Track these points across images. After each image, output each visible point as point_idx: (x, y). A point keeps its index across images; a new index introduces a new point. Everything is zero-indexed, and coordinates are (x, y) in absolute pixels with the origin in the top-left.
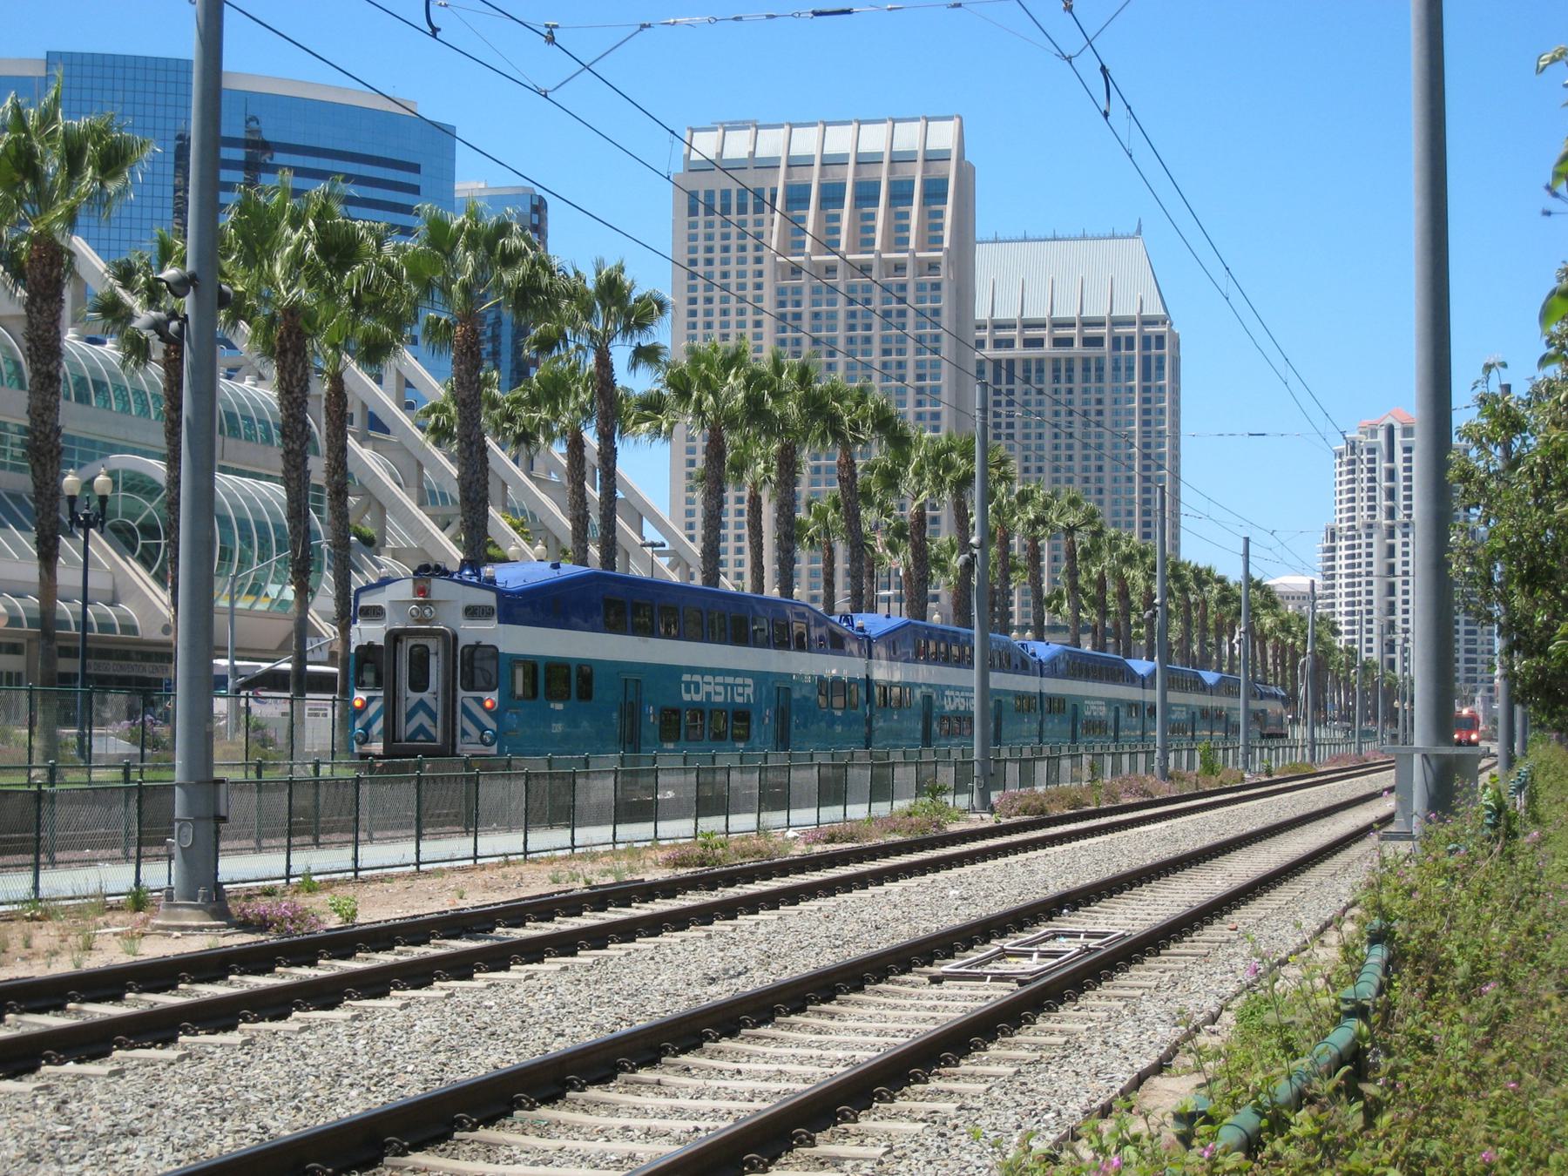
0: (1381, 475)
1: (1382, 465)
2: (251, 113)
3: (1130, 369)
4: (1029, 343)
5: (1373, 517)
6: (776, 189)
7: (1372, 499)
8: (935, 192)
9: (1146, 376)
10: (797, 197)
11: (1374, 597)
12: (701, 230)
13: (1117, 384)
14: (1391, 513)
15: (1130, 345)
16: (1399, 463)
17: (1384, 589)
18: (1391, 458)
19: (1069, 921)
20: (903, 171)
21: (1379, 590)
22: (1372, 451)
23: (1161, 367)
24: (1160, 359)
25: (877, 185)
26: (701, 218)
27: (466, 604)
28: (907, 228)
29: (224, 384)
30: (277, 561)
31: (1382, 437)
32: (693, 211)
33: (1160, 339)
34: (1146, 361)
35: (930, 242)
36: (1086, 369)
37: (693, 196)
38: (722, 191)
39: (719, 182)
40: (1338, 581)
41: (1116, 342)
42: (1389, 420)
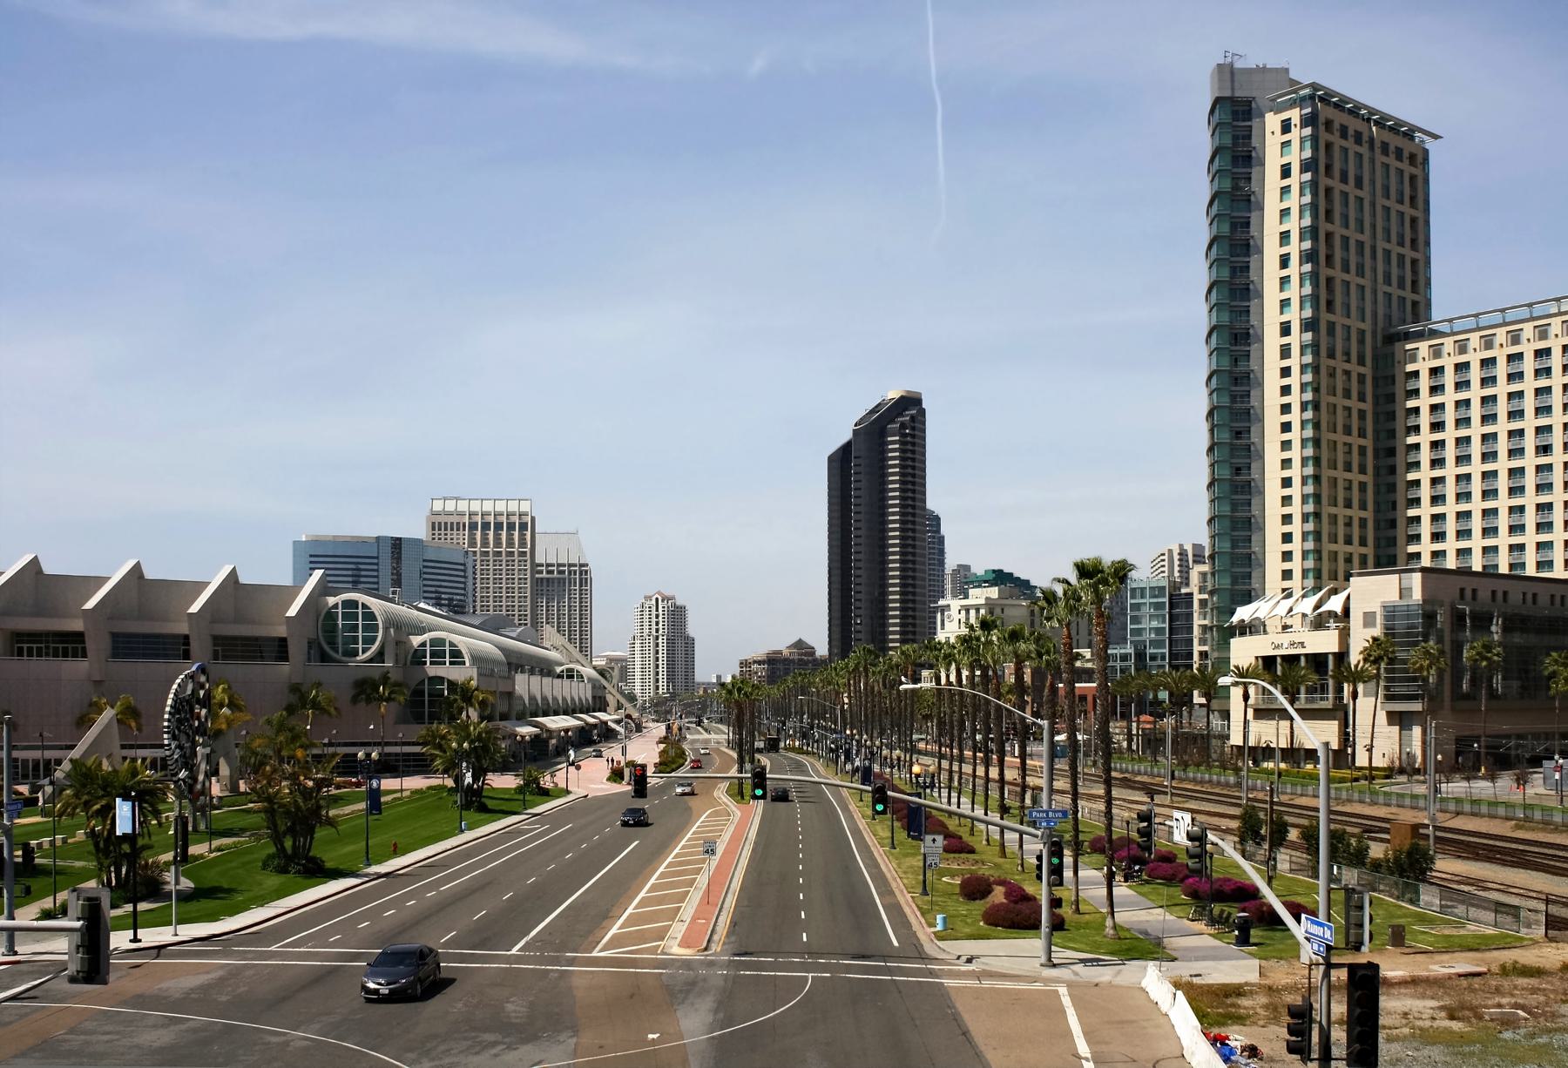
0: (653, 616)
1: (654, 613)
2: (1280, 629)
3: (575, 583)
4: (549, 572)
8: (523, 526)
9: (581, 585)
10: (473, 526)
13: (1557, 737)
14: (657, 631)
15: (575, 574)
18: (657, 610)
19: (716, 937)
20: (500, 519)
23: (586, 582)
24: (586, 579)
26: (437, 532)
27: (1381, 966)
29: (1028, 762)
31: (654, 602)
32: (433, 529)
33: (586, 572)
34: (581, 580)
36: (559, 583)
37: (433, 524)
39: (443, 519)
41: (570, 572)
42: (657, 596)
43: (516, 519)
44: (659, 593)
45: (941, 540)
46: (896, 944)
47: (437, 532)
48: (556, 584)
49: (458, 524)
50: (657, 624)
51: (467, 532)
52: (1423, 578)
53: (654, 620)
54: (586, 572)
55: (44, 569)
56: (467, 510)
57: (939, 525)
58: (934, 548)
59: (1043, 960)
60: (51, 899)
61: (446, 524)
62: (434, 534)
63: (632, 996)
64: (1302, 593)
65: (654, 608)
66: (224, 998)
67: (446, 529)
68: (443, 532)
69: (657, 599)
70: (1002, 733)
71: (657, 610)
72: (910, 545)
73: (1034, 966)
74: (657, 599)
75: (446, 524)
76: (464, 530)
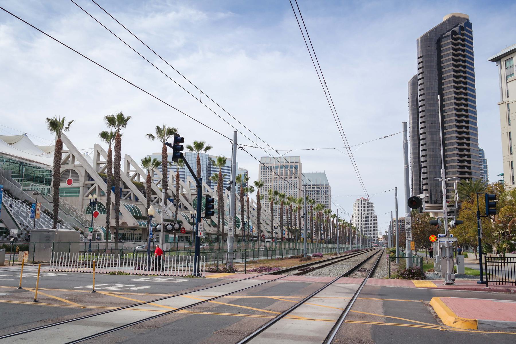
1: (360, 206)
4: (317, 188)
7: (359, 211)
15: (319, 191)
16: (363, 206)
18: (361, 205)
20: (292, 164)
22: (359, 204)
26: (263, 170)
32: (262, 169)
43: (294, 164)
44: (362, 198)
45: (485, 161)
47: (263, 170)
48: (320, 192)
52: (409, 259)
53: (360, 208)
54: (328, 187)
56: (294, 160)
57: (483, 154)
58: (482, 170)
60: (92, 286)
62: (262, 171)
67: (264, 169)
68: (265, 170)
69: (361, 200)
70: (457, 263)
71: (361, 205)
72: (467, 166)
74: (361, 200)
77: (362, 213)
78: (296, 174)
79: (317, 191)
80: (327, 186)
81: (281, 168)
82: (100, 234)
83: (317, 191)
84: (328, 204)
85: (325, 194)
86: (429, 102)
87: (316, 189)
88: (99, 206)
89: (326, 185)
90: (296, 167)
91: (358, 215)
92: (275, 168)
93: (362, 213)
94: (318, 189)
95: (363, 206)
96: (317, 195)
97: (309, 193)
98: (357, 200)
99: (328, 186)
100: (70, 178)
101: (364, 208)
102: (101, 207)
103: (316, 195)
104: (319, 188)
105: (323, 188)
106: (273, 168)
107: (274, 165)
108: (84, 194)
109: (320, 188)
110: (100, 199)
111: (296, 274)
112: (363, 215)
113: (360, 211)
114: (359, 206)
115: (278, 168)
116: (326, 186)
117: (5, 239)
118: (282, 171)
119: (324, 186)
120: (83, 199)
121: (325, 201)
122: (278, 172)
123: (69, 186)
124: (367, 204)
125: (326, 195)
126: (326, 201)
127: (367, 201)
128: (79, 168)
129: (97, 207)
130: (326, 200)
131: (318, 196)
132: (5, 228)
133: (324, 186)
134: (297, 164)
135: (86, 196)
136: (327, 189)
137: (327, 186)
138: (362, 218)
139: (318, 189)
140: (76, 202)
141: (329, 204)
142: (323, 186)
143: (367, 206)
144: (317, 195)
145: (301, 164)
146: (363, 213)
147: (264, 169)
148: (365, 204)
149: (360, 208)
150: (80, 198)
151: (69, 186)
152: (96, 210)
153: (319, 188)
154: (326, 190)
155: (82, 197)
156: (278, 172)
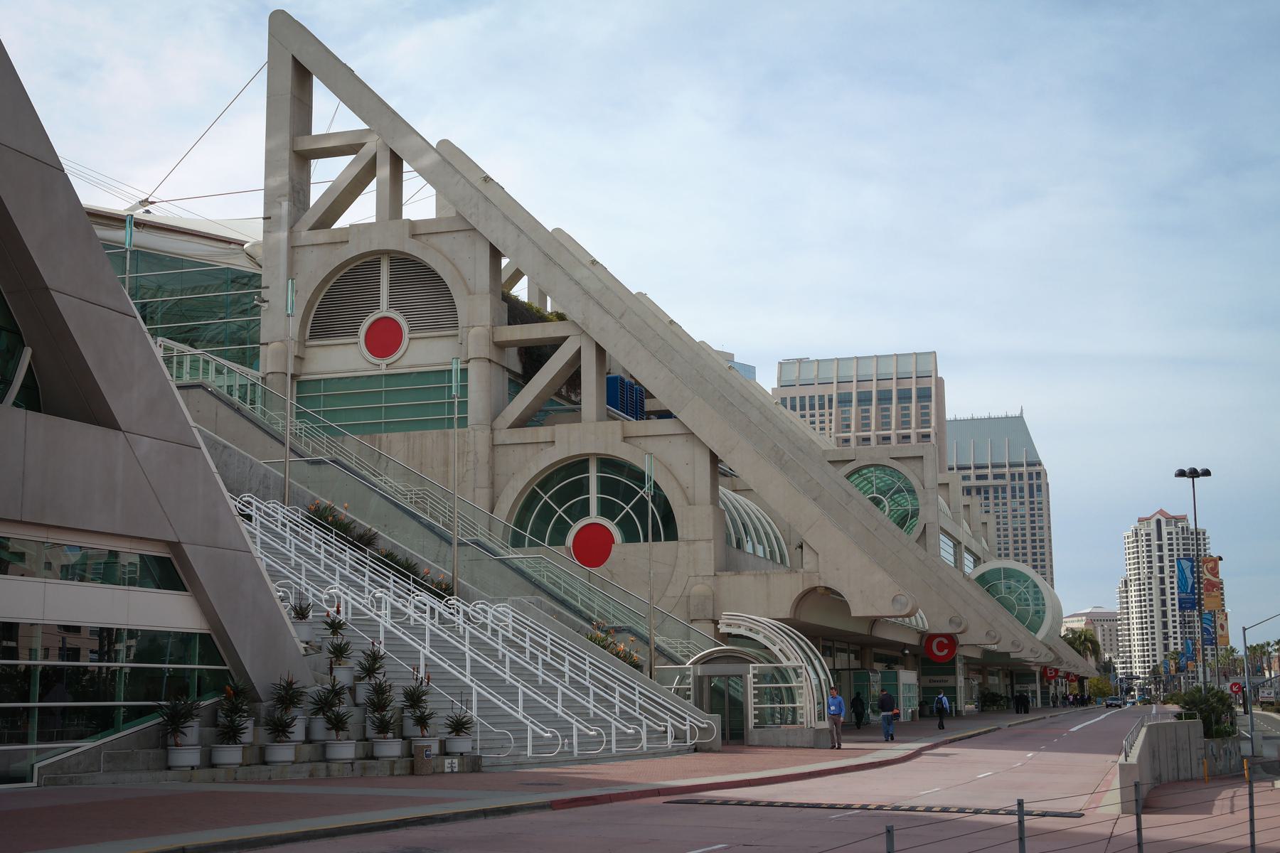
1: (1155, 543)
5: (1152, 573)
6: (832, 395)
7: (1150, 562)
9: (1031, 496)
11: (1157, 653)
12: (817, 419)
15: (1004, 491)
16: (1165, 541)
17: (1162, 636)
18: (1160, 538)
21: (1158, 626)
22: (1148, 535)
25: (891, 391)
28: (889, 417)
30: (464, 654)
31: (1153, 525)
35: (922, 424)
38: (810, 397)
40: (1130, 594)
41: (1013, 476)
42: (1159, 516)
44: (1161, 512)
46: (1072, 730)
49: (821, 398)
50: (1161, 559)
51: (834, 411)
53: (1156, 553)
54: (1038, 474)
55: (82, 202)
59: (388, 773)
61: (802, 399)
63: (513, 474)
64: (652, 478)
65: (1154, 536)
66: (1071, 636)
67: (812, 407)
69: (1159, 522)
71: (1160, 538)
73: (68, 640)
74: (1159, 522)
75: (802, 399)
76: (830, 407)
77: (1162, 570)
78: (925, 422)
79: (996, 489)
80: (1034, 469)
81: (864, 399)
82: (782, 674)
83: (996, 491)
84: (1042, 541)
85: (1027, 499)
86: (456, 426)
87: (990, 481)
88: (605, 485)
89: (1011, 466)
90: (924, 395)
91: (1146, 581)
92: (839, 402)
93: (1162, 570)
94: (1000, 482)
95: (1165, 541)
96: (996, 505)
97: (1000, 494)
98: (1140, 520)
99: (1038, 468)
100: (384, 310)
101: (1171, 550)
102: (628, 494)
103: (992, 505)
104: (1002, 476)
105: (1021, 475)
106: (830, 400)
107: (833, 391)
108: (495, 414)
109: (1008, 477)
110: (619, 437)
111: (632, 783)
112: (1167, 581)
113: (1156, 564)
114: (1148, 546)
115: (871, 400)
116: (1032, 469)
117: (230, 755)
118: (868, 411)
119: (1024, 469)
120: (493, 446)
121: (1028, 525)
122: (853, 416)
123: (382, 366)
124: (1180, 536)
125: (1032, 503)
126: (1033, 528)
127: (1180, 525)
128: (444, 243)
129: (594, 495)
130: (1033, 522)
131: (1001, 508)
132: (205, 638)
133: (1024, 469)
134: (924, 383)
135: (513, 426)
136: (1035, 481)
137: (1034, 469)
138: (1163, 592)
139: (1000, 482)
140: (446, 463)
141: (1046, 537)
142: (1021, 469)
143: (1181, 542)
144: (996, 505)
145: (940, 382)
146: (1167, 571)
147: (812, 407)
148: (1174, 536)
149: (1156, 553)
150: (477, 437)
151: (383, 362)
152: (594, 517)
153: (1002, 476)
154: (1031, 486)
155: (488, 432)
156: (853, 416)
